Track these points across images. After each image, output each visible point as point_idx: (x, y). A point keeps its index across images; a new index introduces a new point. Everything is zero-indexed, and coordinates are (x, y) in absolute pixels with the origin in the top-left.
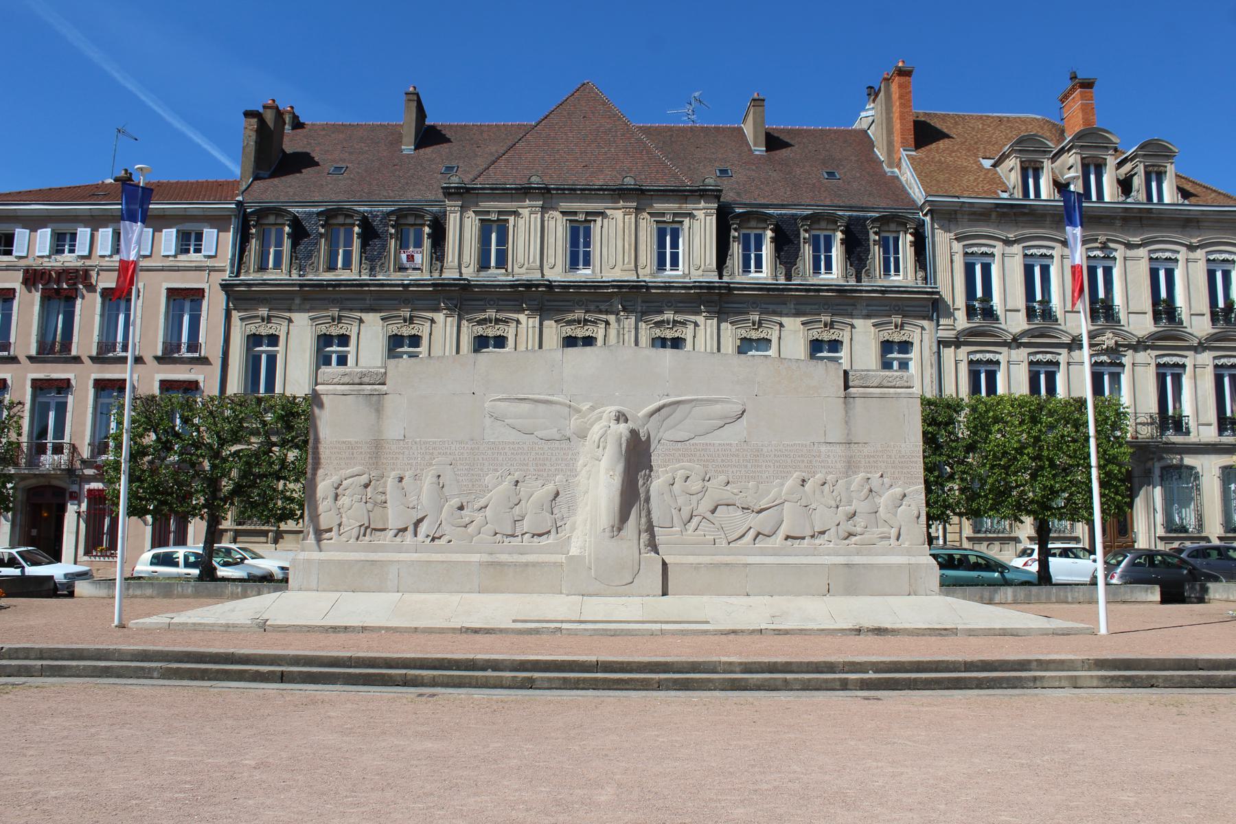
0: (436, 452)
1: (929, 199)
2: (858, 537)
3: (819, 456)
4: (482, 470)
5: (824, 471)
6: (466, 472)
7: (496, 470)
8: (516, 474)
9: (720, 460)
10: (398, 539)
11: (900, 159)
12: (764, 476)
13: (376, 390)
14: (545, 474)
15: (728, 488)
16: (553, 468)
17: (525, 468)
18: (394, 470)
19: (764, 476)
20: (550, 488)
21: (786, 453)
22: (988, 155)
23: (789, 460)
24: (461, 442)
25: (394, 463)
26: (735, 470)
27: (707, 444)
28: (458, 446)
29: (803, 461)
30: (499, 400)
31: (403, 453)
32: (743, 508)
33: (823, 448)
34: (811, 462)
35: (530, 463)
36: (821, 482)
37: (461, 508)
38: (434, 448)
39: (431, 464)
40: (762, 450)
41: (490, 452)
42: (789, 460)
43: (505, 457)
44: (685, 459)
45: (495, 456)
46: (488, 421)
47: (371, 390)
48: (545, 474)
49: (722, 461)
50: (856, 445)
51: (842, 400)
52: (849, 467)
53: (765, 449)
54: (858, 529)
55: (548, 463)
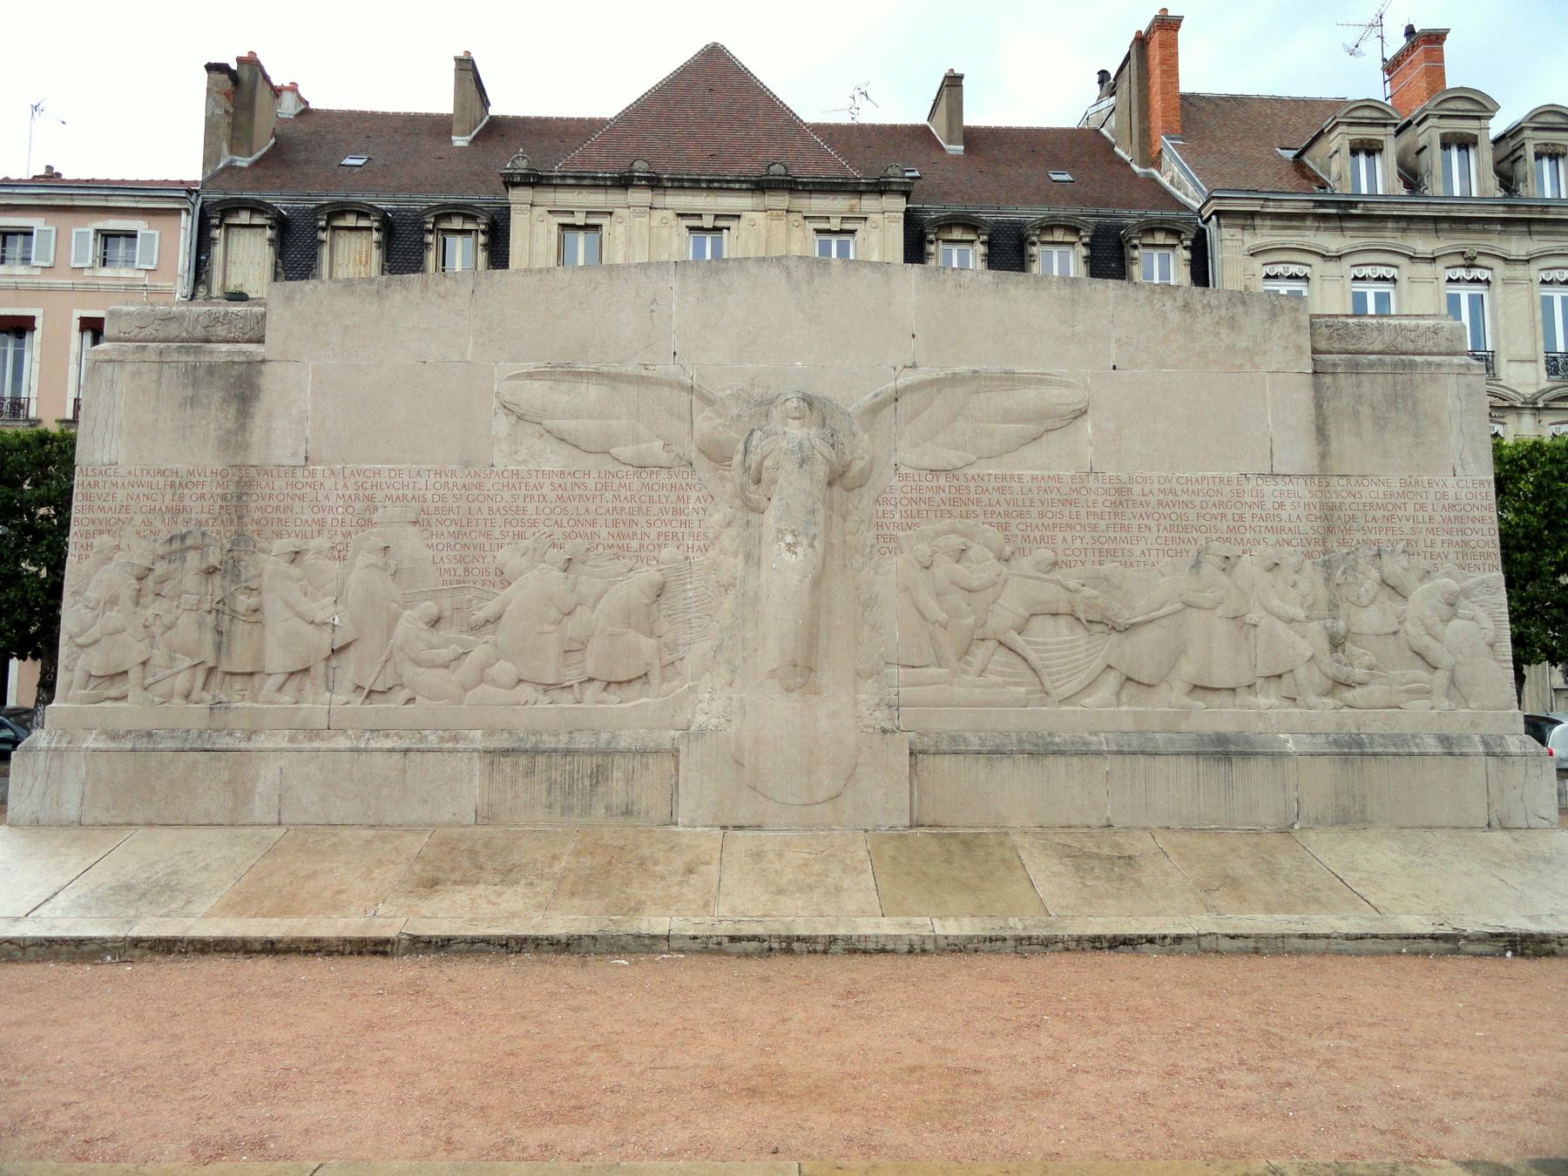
0: (380, 495)
1: (1214, 195)
2: (1358, 691)
3: (1261, 505)
4: (488, 535)
5: (1272, 538)
6: (451, 541)
7: (521, 536)
8: (568, 545)
9: (1034, 511)
10: (286, 699)
11: (1160, 152)
12: (1137, 550)
13: (240, 353)
14: (635, 544)
15: (1056, 575)
16: (653, 532)
17: (589, 530)
18: (279, 535)
19: (1137, 550)
20: (648, 575)
21: (1185, 497)
22: (1287, 144)
23: (1192, 514)
24: (438, 473)
25: (279, 520)
26: (1068, 535)
27: (1004, 477)
28: (432, 480)
29: (1224, 516)
30: (529, 375)
31: (301, 498)
32: (1090, 622)
33: (1269, 487)
34: (1241, 518)
35: (601, 520)
36: (1269, 563)
37: (435, 623)
38: (376, 486)
39: (369, 523)
40: (1130, 490)
41: (506, 494)
42: (1192, 514)
43: (542, 506)
44: (955, 511)
45: (520, 503)
46: (502, 424)
47: (229, 353)
48: (635, 544)
49: (1042, 515)
50: (1343, 481)
51: (1310, 379)
52: (1329, 530)
53: (1137, 489)
54: (1359, 673)
55: (640, 518)
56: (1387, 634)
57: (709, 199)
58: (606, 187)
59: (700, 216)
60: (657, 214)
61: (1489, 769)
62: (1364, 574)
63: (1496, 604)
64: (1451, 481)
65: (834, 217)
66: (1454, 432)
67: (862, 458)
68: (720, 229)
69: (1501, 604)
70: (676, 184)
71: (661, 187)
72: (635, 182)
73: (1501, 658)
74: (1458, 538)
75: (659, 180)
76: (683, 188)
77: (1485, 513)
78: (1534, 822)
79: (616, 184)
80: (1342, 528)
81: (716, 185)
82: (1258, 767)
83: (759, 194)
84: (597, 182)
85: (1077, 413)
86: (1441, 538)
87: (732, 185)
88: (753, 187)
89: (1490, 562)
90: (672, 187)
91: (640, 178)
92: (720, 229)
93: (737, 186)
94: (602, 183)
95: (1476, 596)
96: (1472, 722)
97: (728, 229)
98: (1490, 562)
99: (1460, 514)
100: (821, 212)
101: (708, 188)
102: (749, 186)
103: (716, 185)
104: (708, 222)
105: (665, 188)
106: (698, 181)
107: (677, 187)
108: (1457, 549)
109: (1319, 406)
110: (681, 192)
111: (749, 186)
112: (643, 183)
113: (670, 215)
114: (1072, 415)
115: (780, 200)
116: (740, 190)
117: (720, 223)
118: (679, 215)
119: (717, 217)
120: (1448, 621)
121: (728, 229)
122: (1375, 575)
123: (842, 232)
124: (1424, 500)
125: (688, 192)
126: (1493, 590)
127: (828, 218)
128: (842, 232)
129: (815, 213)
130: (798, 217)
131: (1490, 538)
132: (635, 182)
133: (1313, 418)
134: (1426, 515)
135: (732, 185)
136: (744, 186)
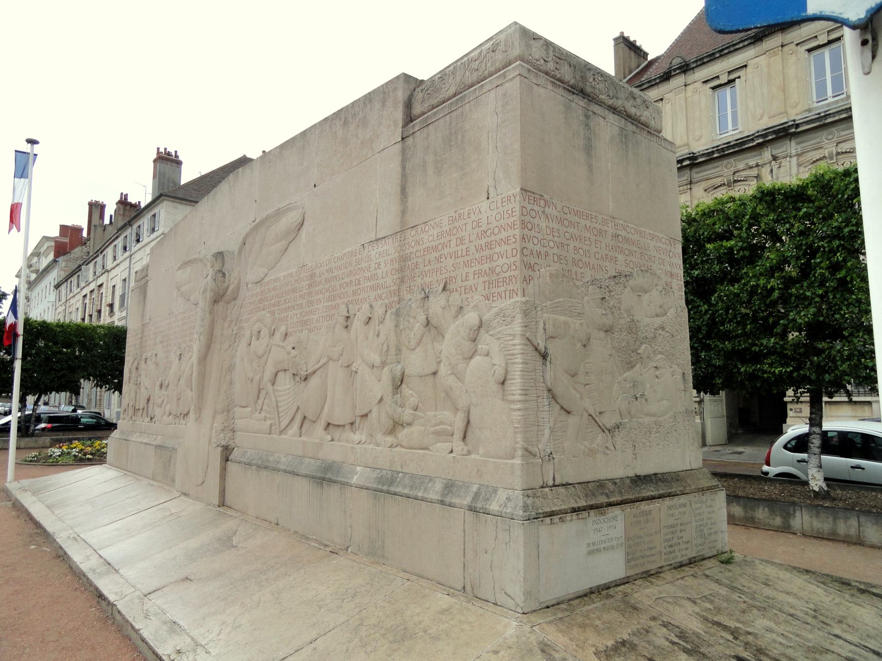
56: (428, 375)
57: (723, 63)
58: (657, 84)
59: (718, 77)
60: (690, 88)
61: (466, 526)
62: (414, 318)
63: (510, 335)
64: (485, 205)
65: (820, 35)
66: (490, 151)
67: (234, 283)
68: (733, 80)
69: (514, 335)
70: (699, 63)
71: (690, 69)
72: (673, 74)
73: (510, 398)
74: (486, 267)
75: (687, 65)
76: (704, 63)
77: (511, 232)
78: (501, 598)
79: (662, 79)
80: (410, 276)
81: (726, 51)
82: (335, 488)
83: (759, 43)
84: (651, 84)
85: (299, 226)
86: (474, 269)
87: (737, 47)
88: (752, 41)
89: (511, 287)
90: (697, 66)
91: (675, 70)
92: (733, 80)
93: (741, 45)
94: (653, 83)
95: (494, 328)
96: (478, 470)
97: (739, 77)
98: (511, 287)
99: (489, 240)
100: (808, 36)
101: (721, 56)
102: (749, 41)
103: (726, 51)
104: (724, 79)
105: (693, 68)
106: (713, 54)
107: (700, 65)
108: (486, 278)
109: (404, 168)
110: (703, 67)
111: (749, 41)
112: (677, 72)
113: (699, 85)
114: (297, 229)
115: (776, 40)
116: (744, 46)
117: (732, 77)
118: (704, 82)
119: (729, 72)
120: (471, 358)
121: (739, 77)
122: (422, 318)
123: (830, 42)
124: (464, 234)
125: (709, 64)
126: (509, 319)
127: (816, 37)
128: (830, 42)
129: (805, 37)
130: (792, 46)
131: (512, 260)
132: (673, 74)
133: (399, 181)
134: (464, 247)
135: (737, 47)
136: (746, 43)
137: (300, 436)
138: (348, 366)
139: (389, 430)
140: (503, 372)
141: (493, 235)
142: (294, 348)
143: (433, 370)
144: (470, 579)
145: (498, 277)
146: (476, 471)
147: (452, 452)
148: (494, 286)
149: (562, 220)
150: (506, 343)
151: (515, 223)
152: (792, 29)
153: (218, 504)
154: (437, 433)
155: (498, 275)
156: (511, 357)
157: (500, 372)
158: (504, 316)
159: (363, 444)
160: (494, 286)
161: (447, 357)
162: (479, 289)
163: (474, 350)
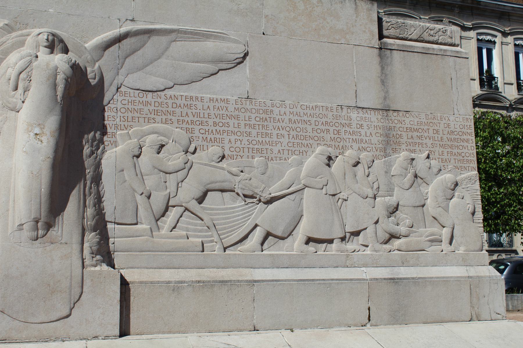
78: (494, 316)
96: (463, 259)
120: (451, 199)
137: (262, 251)
138: (334, 195)
139: (385, 241)
140: (473, 208)
141: (458, 135)
142: (242, 172)
143: (422, 204)
144: (475, 313)
145: (463, 158)
146: (461, 259)
147: (442, 251)
148: (461, 163)
149: (428, 123)
150: (473, 193)
151: (472, 133)
152: (492, 69)
153: (119, 334)
154: (432, 241)
155: (463, 157)
156: (476, 201)
157: (471, 210)
158: (470, 180)
159: (358, 252)
160: (461, 163)
161: (436, 197)
162: (451, 162)
163: (452, 195)
